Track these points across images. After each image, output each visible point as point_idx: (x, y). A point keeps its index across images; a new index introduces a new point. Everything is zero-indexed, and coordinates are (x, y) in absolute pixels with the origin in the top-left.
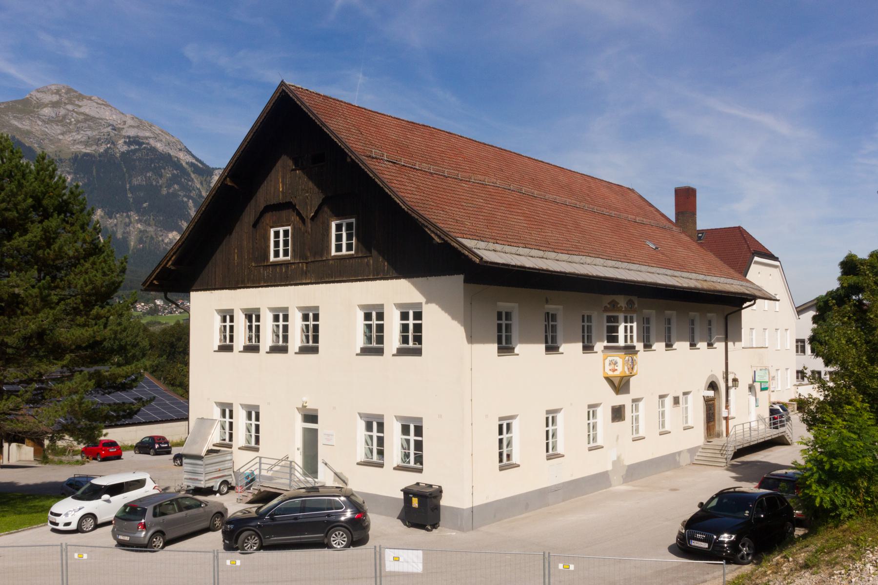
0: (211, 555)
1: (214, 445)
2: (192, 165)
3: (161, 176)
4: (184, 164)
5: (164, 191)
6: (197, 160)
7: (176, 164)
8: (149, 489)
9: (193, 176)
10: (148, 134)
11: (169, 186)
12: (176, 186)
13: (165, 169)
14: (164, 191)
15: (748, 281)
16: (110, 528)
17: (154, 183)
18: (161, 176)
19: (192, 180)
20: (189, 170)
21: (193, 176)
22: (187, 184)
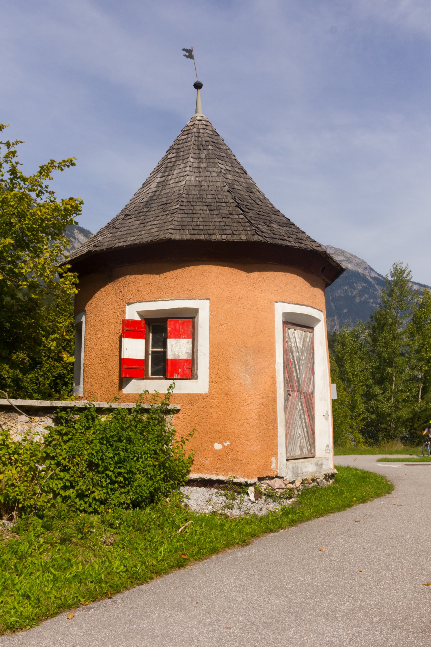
0: (291, 331)
1: (381, 487)
2: (375, 279)
3: (354, 288)
4: (369, 279)
5: (358, 300)
6: (379, 275)
7: (363, 278)
8: (304, 441)
9: (377, 287)
10: (342, 258)
11: (361, 296)
12: (366, 296)
13: (356, 283)
14: (358, 300)
15: (317, 458)
16: (193, 476)
17: (350, 294)
18: (354, 288)
19: (376, 290)
20: (373, 282)
21: (377, 287)
22: (374, 293)
